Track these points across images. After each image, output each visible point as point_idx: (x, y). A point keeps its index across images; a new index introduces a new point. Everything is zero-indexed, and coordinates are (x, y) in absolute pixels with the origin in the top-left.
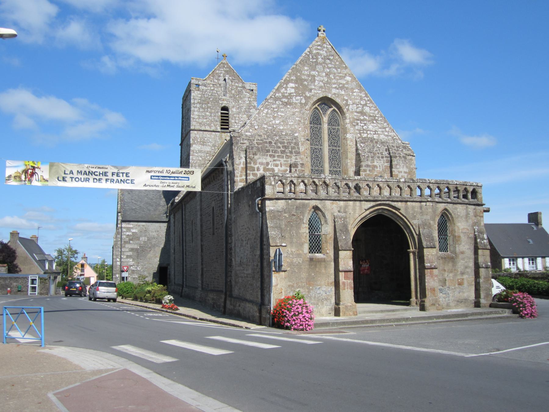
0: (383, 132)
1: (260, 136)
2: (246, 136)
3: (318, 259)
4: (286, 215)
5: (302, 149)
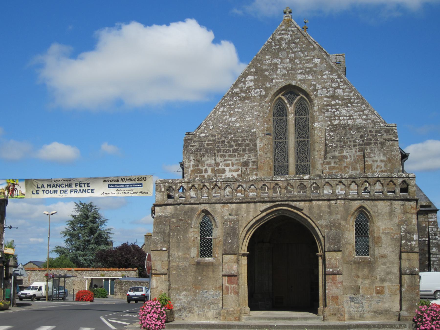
0: (359, 115)
1: (213, 136)
2: (199, 137)
3: (206, 263)
4: (175, 220)
5: (259, 144)
